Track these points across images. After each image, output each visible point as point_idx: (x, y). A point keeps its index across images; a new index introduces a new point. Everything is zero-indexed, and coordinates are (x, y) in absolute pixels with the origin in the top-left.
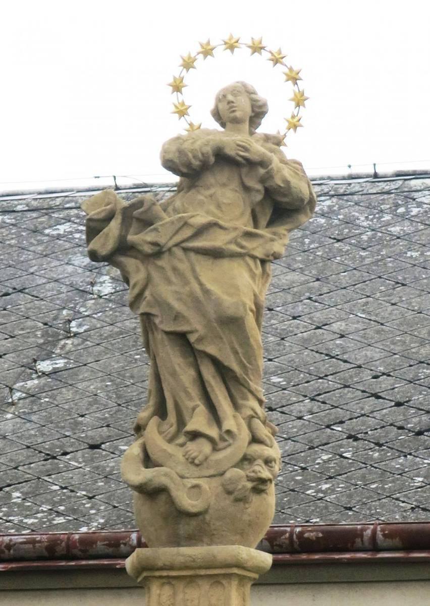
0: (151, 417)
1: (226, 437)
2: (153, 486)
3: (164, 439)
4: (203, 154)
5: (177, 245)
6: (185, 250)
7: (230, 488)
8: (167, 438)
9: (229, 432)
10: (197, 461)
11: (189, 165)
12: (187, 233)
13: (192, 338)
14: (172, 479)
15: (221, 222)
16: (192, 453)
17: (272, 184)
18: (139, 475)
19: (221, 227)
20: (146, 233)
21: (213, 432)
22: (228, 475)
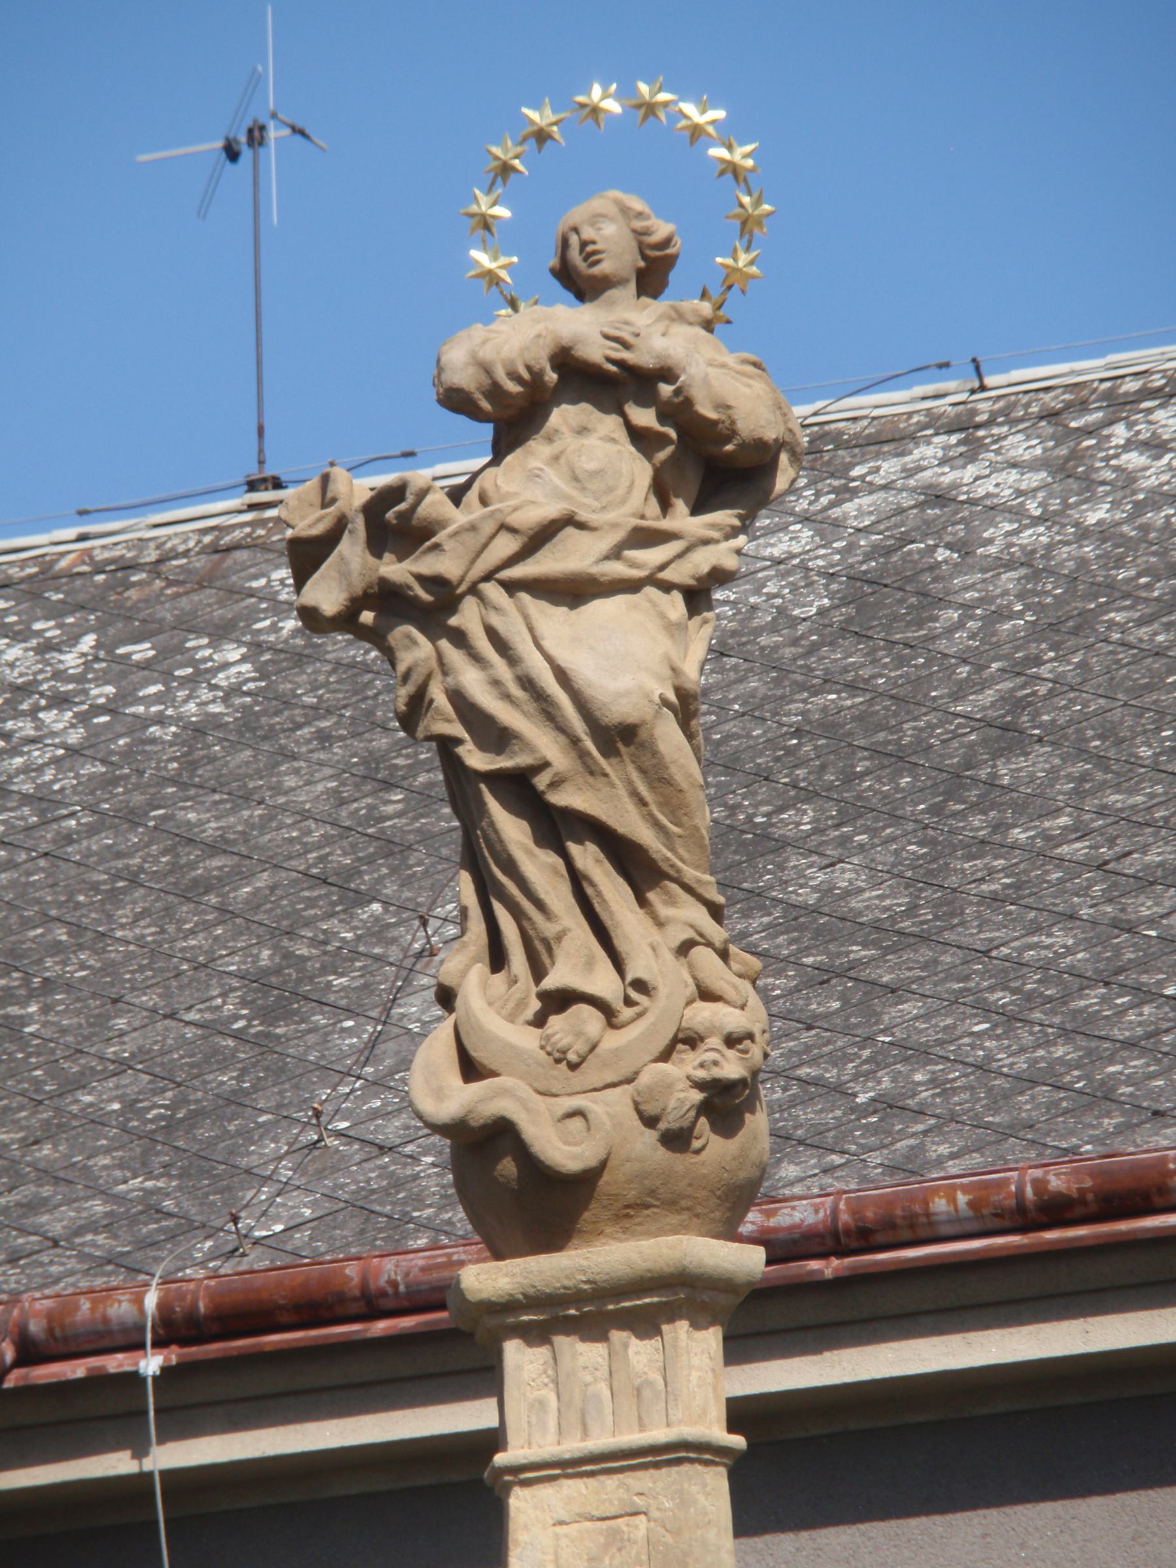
0: (695, 978)
1: (634, 995)
2: (482, 1121)
3: (499, 1013)
4: (529, 368)
5: (488, 577)
6: (512, 587)
7: (650, 1109)
8: (504, 1012)
9: (640, 986)
10: (572, 1057)
11: (495, 391)
12: (506, 545)
13: (541, 781)
14: (521, 1101)
15: (583, 515)
16: (561, 1039)
17: (546, 358)
18: (449, 1097)
19: (582, 526)
20: (418, 557)
21: (603, 982)
22: (644, 1079)
